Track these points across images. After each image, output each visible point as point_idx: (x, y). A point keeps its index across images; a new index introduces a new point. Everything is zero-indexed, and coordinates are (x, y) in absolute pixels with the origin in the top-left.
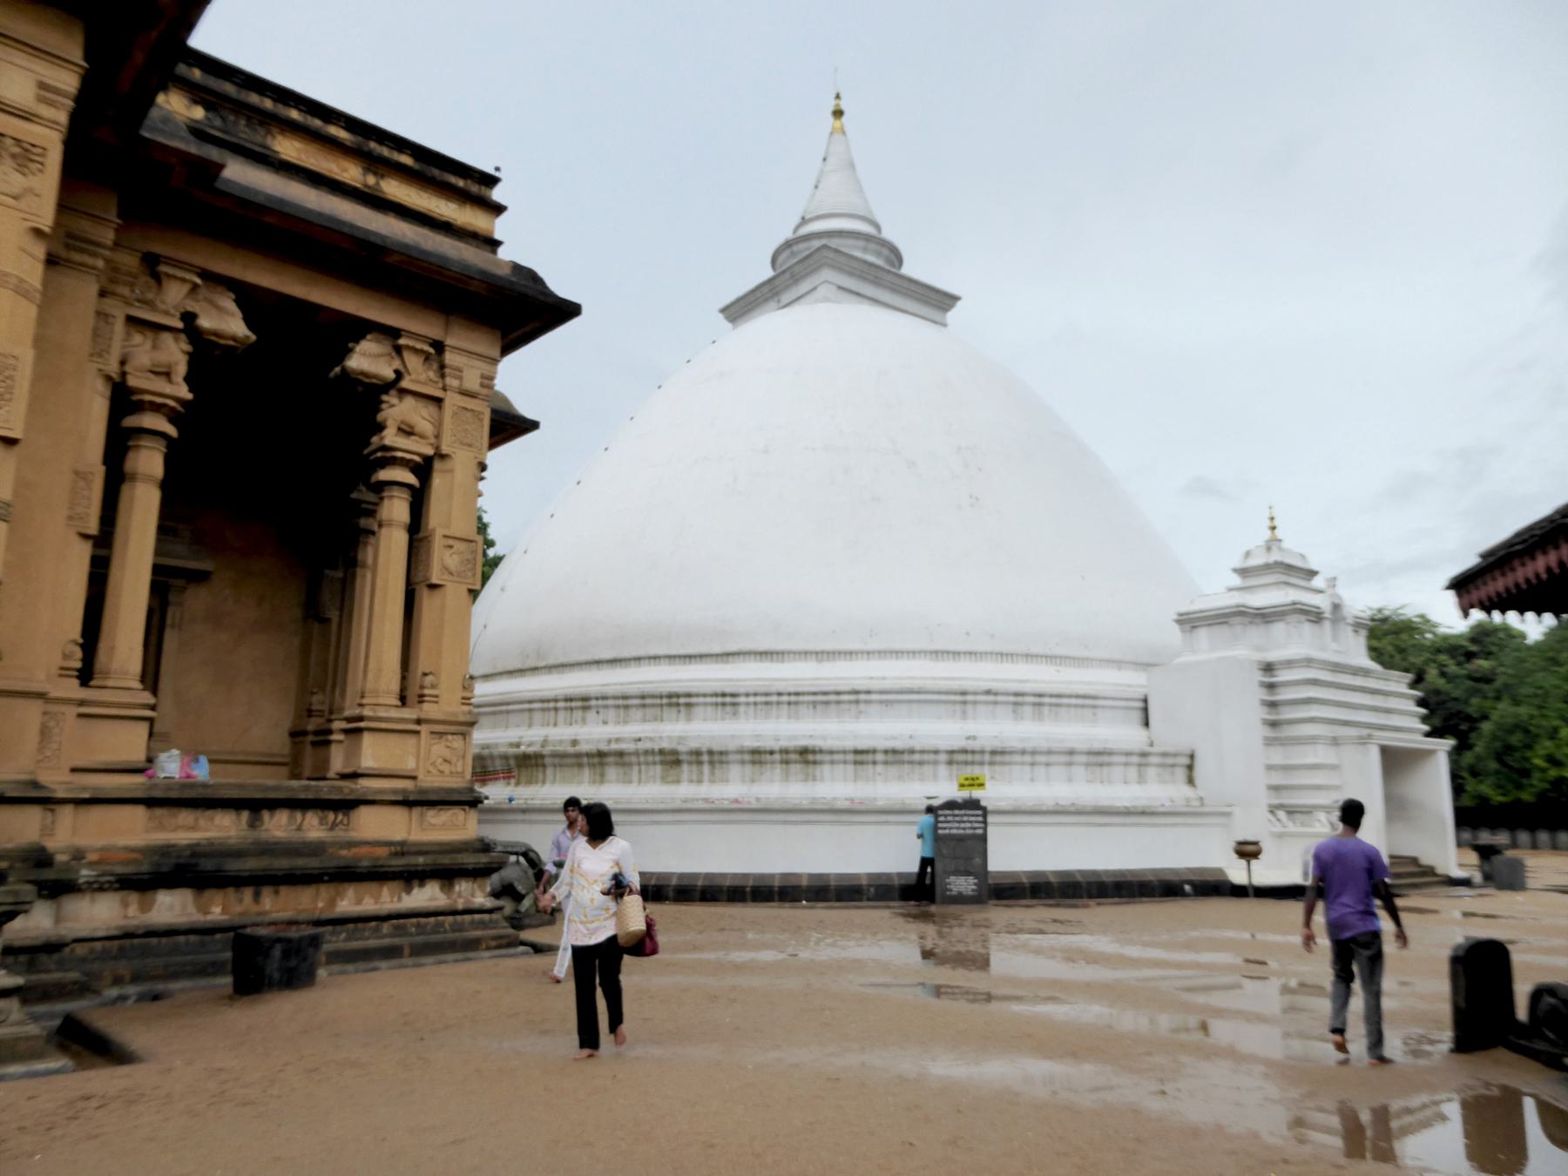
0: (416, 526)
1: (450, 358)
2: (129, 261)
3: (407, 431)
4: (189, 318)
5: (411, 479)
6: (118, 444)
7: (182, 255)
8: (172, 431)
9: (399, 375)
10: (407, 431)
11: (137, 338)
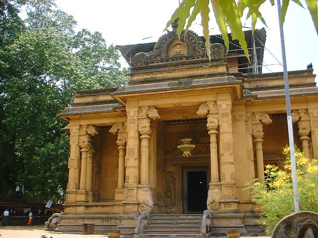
0: (218, 142)
1: (219, 103)
2: (249, 115)
3: (304, 129)
4: (261, 121)
5: (308, 138)
6: (255, 144)
7: (257, 111)
8: (149, 137)
9: (209, 111)
10: (304, 129)
11: (254, 126)
